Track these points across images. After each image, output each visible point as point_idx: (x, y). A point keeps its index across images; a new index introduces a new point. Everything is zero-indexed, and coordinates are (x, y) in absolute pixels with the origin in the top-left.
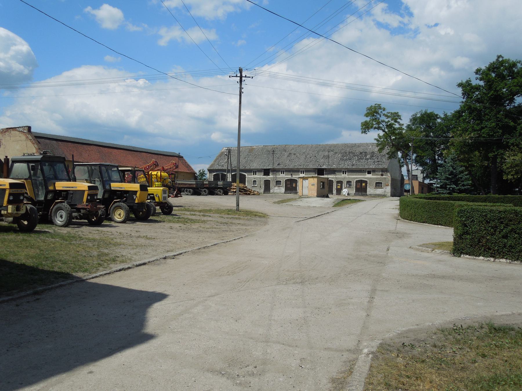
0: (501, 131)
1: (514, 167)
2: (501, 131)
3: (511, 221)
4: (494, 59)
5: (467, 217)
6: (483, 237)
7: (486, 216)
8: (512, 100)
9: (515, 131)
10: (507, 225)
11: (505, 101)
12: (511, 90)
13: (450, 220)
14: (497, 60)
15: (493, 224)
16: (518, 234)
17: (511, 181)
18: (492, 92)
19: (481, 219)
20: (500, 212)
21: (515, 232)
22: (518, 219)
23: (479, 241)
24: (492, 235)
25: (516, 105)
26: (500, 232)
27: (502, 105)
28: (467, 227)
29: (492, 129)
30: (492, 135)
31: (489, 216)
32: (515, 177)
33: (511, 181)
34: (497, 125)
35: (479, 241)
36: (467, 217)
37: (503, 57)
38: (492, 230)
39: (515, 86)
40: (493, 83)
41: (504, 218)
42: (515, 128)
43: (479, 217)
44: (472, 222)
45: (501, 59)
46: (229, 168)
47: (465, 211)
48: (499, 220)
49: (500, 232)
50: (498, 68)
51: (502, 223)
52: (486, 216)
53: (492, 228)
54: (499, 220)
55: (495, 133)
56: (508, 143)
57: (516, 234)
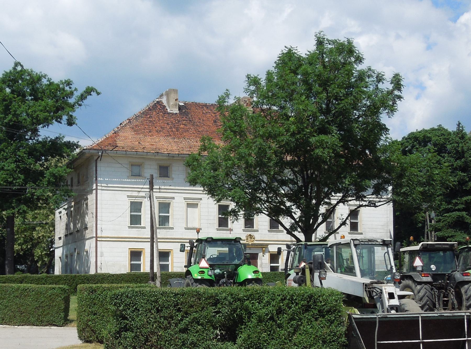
0: (22, 177)
1: (22, 232)
2: (22, 177)
3: (192, 306)
4: (9, 67)
5: (126, 305)
6: (153, 333)
7: (156, 301)
8: (35, 132)
9: (41, 178)
10: (186, 313)
11: (27, 132)
12: (38, 116)
13: (11, 314)
14: (14, 69)
15: (166, 313)
16: (202, 325)
17: (18, 254)
18: (10, 116)
19: (149, 307)
20: (176, 295)
21: (198, 323)
22: (201, 304)
23: (147, 340)
24: (166, 329)
25: (40, 140)
26: (176, 325)
27: (22, 138)
28: (126, 318)
29: (11, 173)
30: (11, 183)
31: (160, 302)
32: (24, 247)
33: (18, 254)
34: (18, 167)
35: (147, 340)
36: (126, 305)
37: (22, 66)
38: (166, 322)
39: (41, 111)
40: (11, 102)
41: (182, 303)
42: (42, 174)
43: (146, 303)
44: (134, 311)
45: (19, 68)
46: (154, 190)
47: (122, 295)
48: (175, 306)
49: (176, 325)
50: (15, 81)
51: (179, 310)
52: (156, 301)
53: (165, 318)
54: (175, 306)
55: (14, 179)
56: (33, 194)
57: (199, 325)
